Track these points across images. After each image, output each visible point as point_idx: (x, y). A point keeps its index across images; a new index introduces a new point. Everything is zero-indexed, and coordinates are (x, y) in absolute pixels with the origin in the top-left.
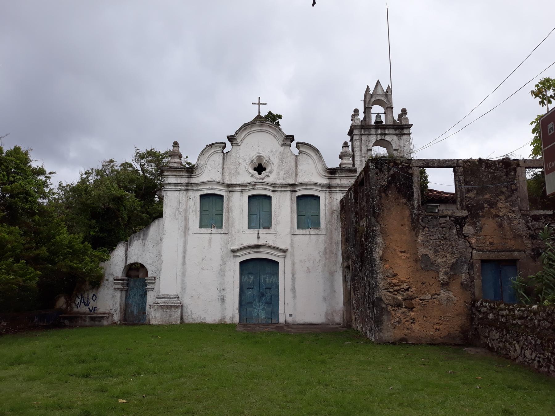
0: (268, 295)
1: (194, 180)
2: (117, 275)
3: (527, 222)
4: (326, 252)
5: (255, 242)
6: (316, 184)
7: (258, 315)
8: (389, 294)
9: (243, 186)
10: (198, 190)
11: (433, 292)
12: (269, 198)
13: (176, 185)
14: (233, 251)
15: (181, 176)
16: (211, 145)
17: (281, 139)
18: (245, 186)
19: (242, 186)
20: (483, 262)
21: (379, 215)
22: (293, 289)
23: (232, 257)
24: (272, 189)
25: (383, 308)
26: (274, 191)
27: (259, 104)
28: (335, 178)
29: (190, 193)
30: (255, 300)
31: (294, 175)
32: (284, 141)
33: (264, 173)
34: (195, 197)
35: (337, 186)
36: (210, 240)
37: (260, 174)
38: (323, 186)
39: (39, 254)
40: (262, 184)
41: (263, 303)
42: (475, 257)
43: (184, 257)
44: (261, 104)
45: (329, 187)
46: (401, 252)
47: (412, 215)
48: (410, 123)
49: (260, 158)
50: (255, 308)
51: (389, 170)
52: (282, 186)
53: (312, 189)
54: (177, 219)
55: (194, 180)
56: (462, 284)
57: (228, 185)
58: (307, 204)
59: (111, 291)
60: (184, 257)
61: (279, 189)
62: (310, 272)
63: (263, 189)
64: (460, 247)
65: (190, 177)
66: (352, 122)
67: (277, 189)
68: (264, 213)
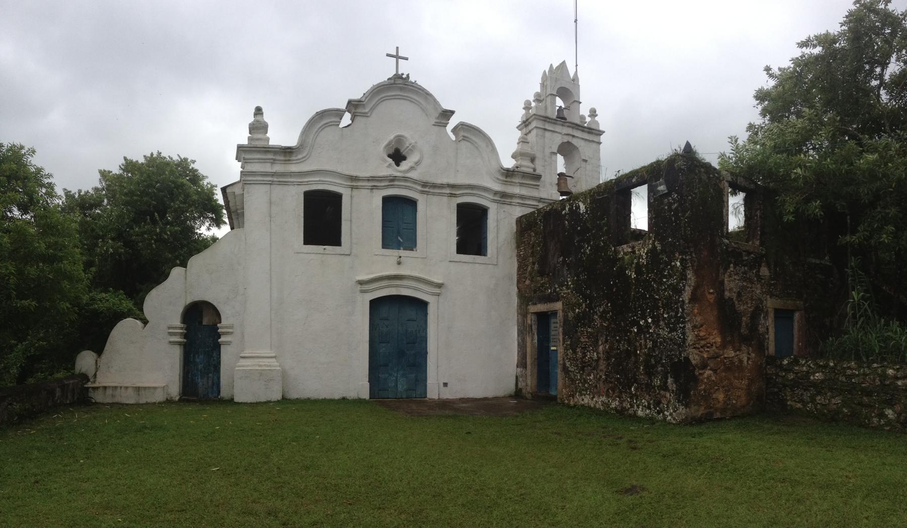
6: (486, 189)
9: (374, 182)
12: (413, 203)
14: (361, 283)
24: (419, 188)
26: (422, 192)
27: (397, 57)
28: (512, 184)
33: (404, 165)
37: (398, 165)
38: (496, 193)
39: (747, 325)
45: (504, 195)
49: (399, 139)
53: (480, 196)
58: (471, 231)
61: (432, 190)
67: (426, 189)
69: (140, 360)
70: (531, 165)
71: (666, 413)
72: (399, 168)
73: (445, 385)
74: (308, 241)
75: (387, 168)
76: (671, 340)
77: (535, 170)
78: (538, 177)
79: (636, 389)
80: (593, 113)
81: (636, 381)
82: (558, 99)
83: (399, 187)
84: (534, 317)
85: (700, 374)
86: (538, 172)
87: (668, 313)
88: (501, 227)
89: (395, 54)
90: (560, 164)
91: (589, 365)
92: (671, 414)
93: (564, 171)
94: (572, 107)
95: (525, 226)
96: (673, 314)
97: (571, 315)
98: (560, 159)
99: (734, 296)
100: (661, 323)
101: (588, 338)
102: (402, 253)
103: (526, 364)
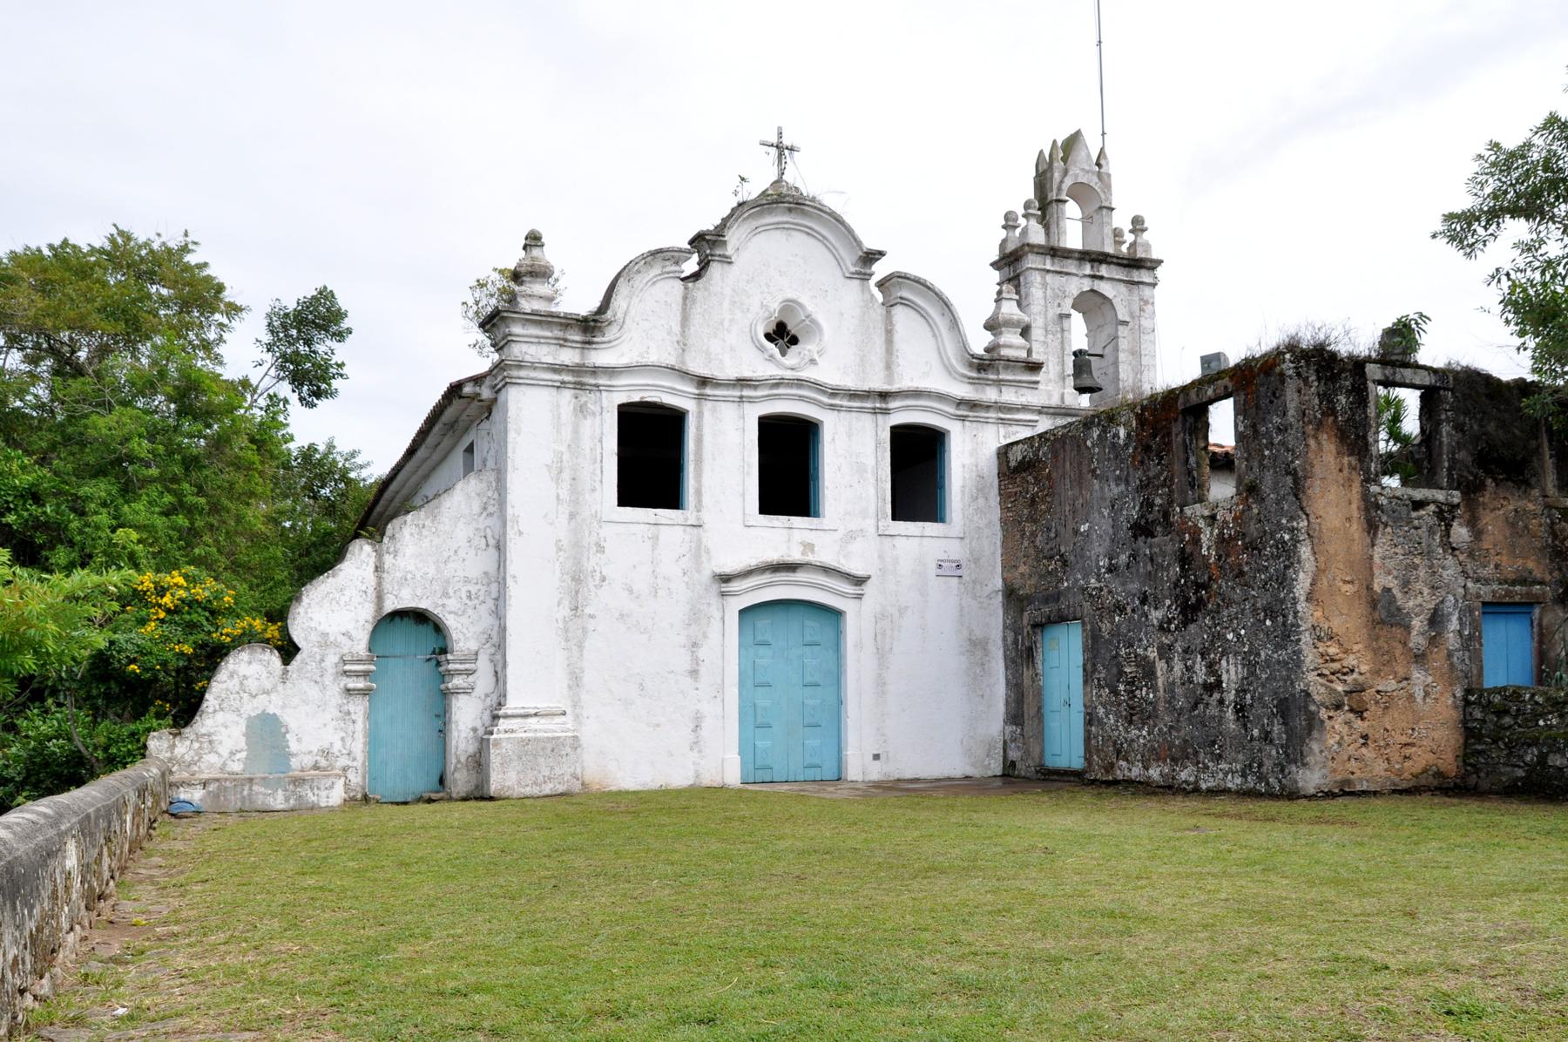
1: (600, 358)
6: (941, 397)
8: (1320, 680)
11: (1401, 671)
14: (726, 579)
15: (563, 343)
22: (881, 684)
25: (1312, 713)
26: (832, 407)
38: (961, 403)
40: (800, 383)
45: (973, 405)
46: (1345, 582)
48: (1154, 256)
49: (790, 306)
55: (600, 358)
57: (703, 382)
63: (801, 398)
64: (1445, 574)
66: (1003, 233)
67: (837, 401)
69: (287, 716)
70: (1020, 341)
73: (876, 757)
74: (625, 499)
75: (761, 362)
77: (1029, 352)
78: (1034, 367)
80: (1138, 225)
85: (1330, 718)
86: (1036, 357)
88: (970, 456)
89: (775, 141)
90: (1078, 335)
93: (1085, 347)
98: (1077, 322)
99: (1391, 582)
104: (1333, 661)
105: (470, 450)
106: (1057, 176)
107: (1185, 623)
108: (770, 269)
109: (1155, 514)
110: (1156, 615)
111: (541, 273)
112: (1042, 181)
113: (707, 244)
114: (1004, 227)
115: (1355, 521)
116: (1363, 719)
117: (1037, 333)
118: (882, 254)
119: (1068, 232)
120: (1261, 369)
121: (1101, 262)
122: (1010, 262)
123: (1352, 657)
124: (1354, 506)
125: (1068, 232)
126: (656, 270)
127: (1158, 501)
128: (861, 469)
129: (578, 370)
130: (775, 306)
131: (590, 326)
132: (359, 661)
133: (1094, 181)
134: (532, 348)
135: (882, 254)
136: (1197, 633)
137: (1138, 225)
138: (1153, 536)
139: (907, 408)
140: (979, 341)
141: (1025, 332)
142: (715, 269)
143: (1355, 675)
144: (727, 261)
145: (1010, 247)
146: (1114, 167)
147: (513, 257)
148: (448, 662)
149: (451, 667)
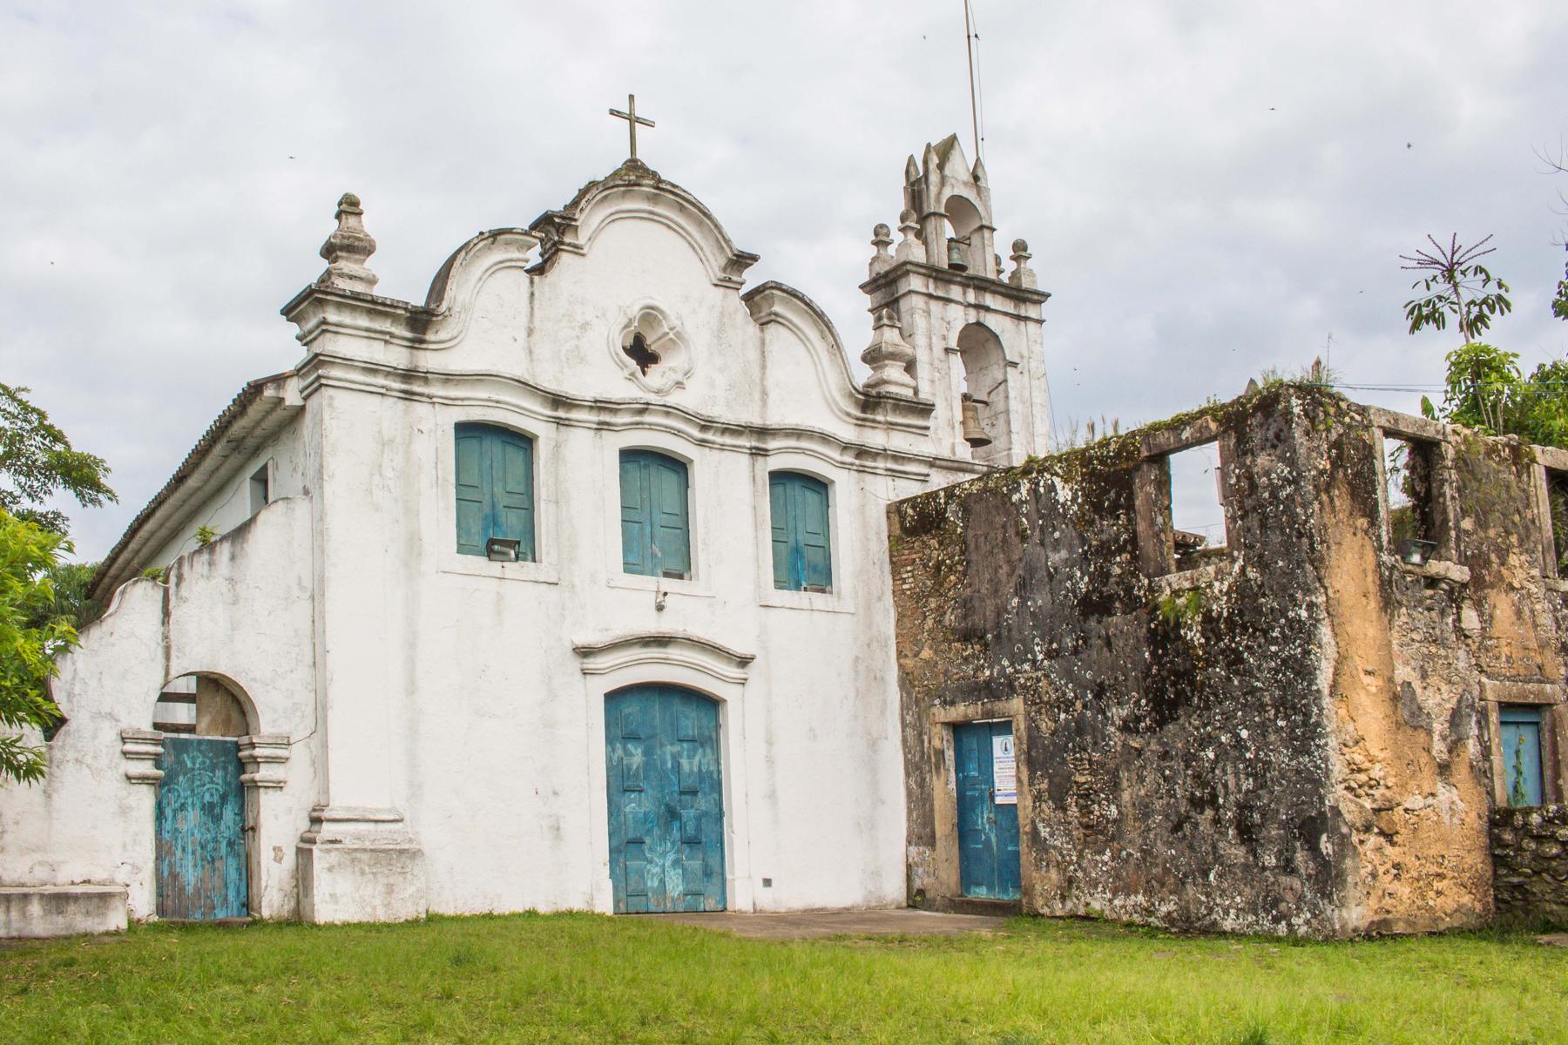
0: (688, 814)
1: (428, 360)
2: (135, 724)
3: (1555, 609)
4: (856, 672)
5: (652, 625)
6: (825, 438)
7: (662, 882)
10: (449, 402)
11: (1427, 789)
13: (372, 369)
14: (585, 652)
15: (387, 338)
16: (495, 235)
17: (717, 262)
18: (611, 411)
19: (601, 409)
20: (1505, 707)
21: (1322, 560)
23: (579, 675)
25: (1343, 836)
26: (702, 443)
27: (633, 120)
29: (421, 409)
30: (649, 832)
31: (757, 396)
32: (724, 270)
34: (433, 428)
35: (883, 453)
36: (500, 598)
38: (846, 447)
40: (668, 411)
41: (673, 843)
42: (1490, 695)
43: (411, 663)
44: (638, 120)
45: (862, 452)
46: (1368, 673)
47: (1379, 566)
48: (1040, 288)
49: (650, 315)
50: (651, 862)
51: (1328, 430)
52: (727, 430)
54: (377, 509)
55: (428, 360)
56: (1472, 767)
57: (558, 401)
59: (112, 785)
60: (411, 663)
62: (815, 736)
65: (417, 343)
66: (873, 251)
67: (709, 436)
68: (665, 519)
70: (907, 379)
71: (1294, 921)
72: (647, 380)
73: (767, 882)
76: (1298, 772)
77: (916, 392)
78: (925, 410)
79: (1220, 876)
80: (1020, 250)
81: (1218, 859)
82: (946, 223)
83: (651, 427)
84: (947, 735)
85: (1362, 842)
86: (924, 395)
87: (1287, 717)
91: (1101, 832)
92: (1307, 922)
94: (975, 240)
95: (917, 523)
96: (1299, 718)
97: (1046, 725)
100: (1272, 738)
101: (1093, 773)
102: (668, 584)
103: (933, 836)
104: (1360, 771)
105: (261, 479)
106: (933, 189)
107: (1161, 722)
108: (631, 264)
109: (1112, 588)
110: (1118, 713)
111: (357, 247)
112: (916, 192)
113: (554, 232)
114: (876, 243)
115: (1371, 597)
116: (1393, 844)
117: (923, 370)
118: (754, 258)
119: (946, 250)
120: (1256, 408)
121: (985, 290)
122: (885, 287)
123: (1378, 766)
124: (1370, 579)
125: (946, 250)
126: (497, 255)
127: (1117, 570)
128: (179, 650)
129: (409, 375)
130: (635, 311)
131: (421, 321)
132: (144, 740)
133: (970, 194)
134: (352, 342)
135: (754, 258)
136: (1180, 732)
137: (1020, 250)
138: (1110, 615)
139: (786, 450)
140: (863, 375)
141: (910, 367)
142: (565, 259)
143: (1382, 790)
144: (577, 250)
145: (882, 268)
146: (993, 177)
147: (328, 228)
148: (253, 745)
149: (258, 752)
